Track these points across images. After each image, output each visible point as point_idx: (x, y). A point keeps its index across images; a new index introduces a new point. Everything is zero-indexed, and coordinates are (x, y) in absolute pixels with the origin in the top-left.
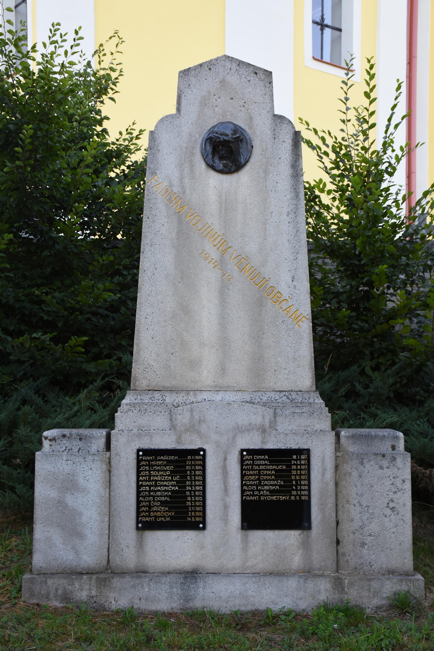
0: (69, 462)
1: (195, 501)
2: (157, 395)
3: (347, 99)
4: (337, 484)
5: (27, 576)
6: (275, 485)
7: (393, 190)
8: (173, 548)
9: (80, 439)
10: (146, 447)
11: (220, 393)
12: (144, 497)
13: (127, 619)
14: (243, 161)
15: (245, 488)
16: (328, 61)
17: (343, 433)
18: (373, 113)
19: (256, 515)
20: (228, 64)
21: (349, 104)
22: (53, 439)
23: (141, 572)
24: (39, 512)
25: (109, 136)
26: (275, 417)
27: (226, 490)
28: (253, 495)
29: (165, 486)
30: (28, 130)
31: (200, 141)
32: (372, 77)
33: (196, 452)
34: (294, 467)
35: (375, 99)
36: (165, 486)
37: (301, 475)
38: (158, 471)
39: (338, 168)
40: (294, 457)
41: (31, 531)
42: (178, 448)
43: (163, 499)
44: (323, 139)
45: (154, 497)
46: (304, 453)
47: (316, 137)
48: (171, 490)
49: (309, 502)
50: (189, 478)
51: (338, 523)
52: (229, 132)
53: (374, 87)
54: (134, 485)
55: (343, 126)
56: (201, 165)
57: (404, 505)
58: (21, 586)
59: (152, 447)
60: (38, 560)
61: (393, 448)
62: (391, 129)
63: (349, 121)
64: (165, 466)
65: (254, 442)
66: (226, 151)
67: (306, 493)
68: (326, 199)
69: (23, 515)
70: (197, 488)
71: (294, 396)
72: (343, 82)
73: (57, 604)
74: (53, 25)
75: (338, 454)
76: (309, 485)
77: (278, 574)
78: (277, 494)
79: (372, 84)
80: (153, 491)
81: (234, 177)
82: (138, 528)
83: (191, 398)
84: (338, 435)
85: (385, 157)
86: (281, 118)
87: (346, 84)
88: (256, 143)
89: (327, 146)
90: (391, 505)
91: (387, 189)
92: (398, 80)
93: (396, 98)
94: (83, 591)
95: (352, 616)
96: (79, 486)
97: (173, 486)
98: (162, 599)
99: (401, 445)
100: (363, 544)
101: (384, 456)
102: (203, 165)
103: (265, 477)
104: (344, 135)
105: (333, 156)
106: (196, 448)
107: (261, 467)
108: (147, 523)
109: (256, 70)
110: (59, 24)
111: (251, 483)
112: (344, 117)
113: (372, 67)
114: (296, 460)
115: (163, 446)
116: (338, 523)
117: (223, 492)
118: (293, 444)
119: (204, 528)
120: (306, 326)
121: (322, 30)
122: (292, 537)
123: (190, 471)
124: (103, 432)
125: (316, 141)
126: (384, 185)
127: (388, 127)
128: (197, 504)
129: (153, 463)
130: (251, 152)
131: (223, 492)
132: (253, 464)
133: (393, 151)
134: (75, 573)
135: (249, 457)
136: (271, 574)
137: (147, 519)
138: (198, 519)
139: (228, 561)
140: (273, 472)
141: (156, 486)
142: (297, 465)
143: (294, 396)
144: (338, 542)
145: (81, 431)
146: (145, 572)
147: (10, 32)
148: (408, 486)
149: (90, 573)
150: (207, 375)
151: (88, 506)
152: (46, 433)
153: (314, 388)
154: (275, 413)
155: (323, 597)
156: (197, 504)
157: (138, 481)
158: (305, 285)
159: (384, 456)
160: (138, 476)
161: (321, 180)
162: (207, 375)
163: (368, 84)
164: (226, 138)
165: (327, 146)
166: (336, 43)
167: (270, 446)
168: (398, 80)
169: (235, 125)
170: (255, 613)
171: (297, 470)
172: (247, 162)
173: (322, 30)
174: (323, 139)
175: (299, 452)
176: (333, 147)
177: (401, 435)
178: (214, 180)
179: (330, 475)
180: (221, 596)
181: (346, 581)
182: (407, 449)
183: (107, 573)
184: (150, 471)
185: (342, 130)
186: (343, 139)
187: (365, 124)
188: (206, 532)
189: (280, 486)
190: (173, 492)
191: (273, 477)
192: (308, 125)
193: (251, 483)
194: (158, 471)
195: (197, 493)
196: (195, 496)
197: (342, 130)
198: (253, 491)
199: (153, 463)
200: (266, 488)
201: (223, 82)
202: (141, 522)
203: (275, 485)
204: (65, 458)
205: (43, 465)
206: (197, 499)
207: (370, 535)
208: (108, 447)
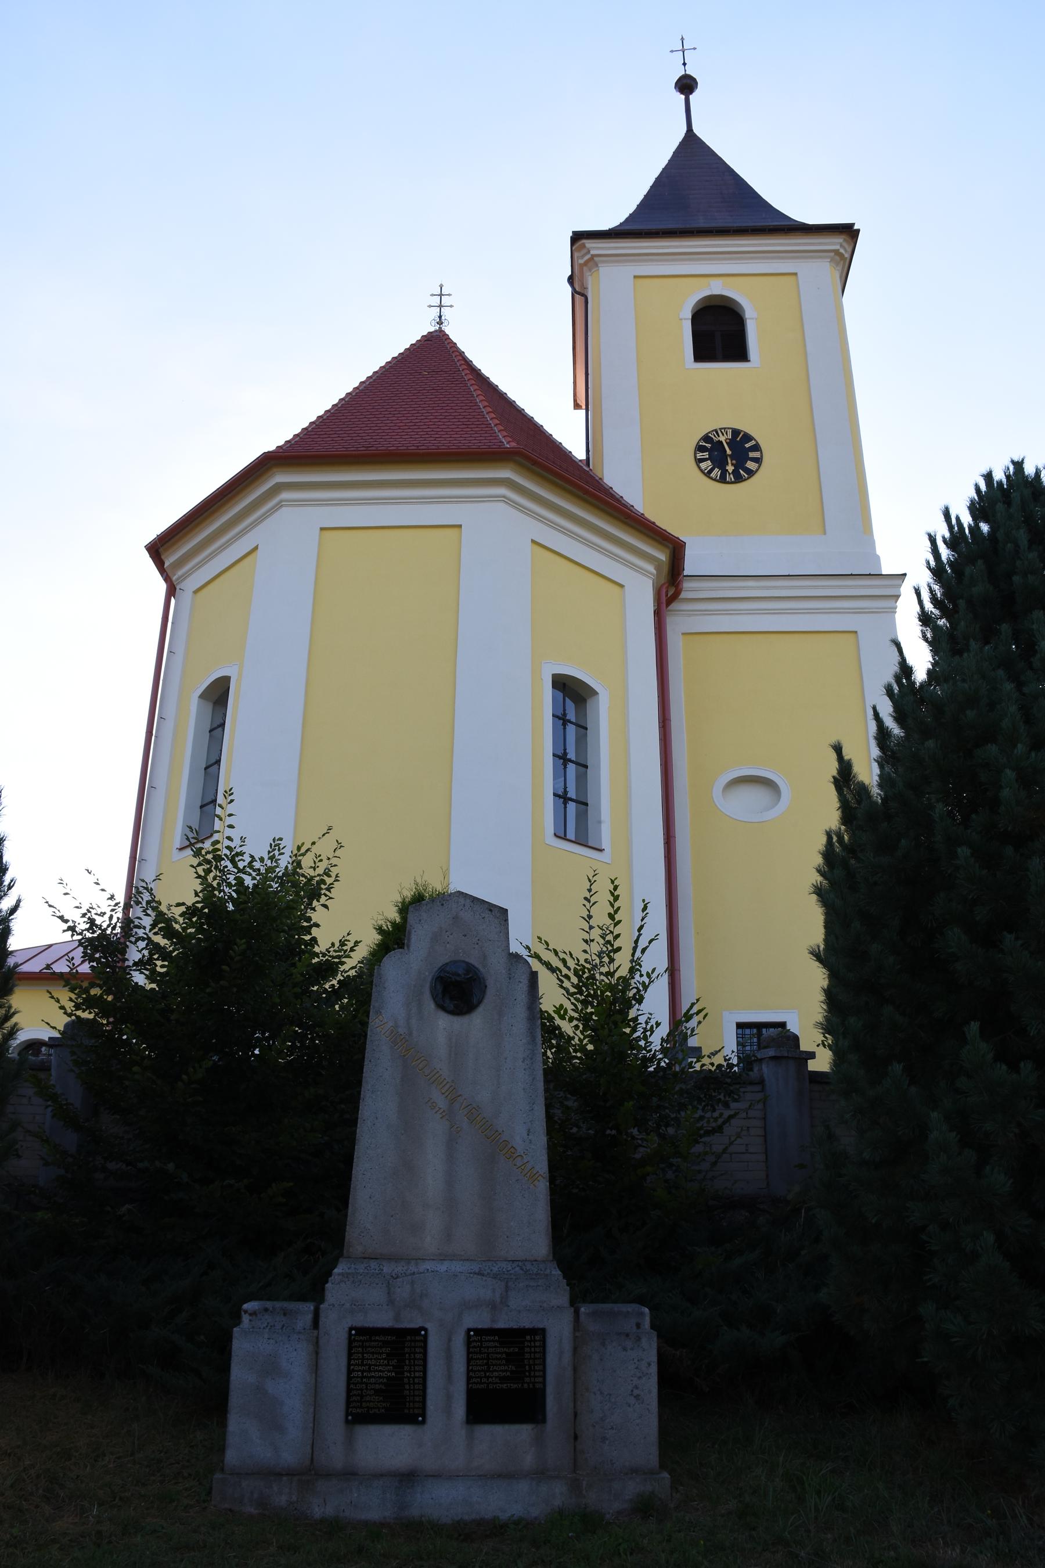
0: (272, 1341)
1: (414, 1390)
2: (373, 1264)
3: (590, 917)
4: (575, 1369)
5: (218, 1476)
6: (506, 1371)
7: (642, 1020)
8: (388, 1446)
9: (285, 1314)
10: (359, 1325)
11: (446, 1262)
12: (355, 1384)
13: (333, 1527)
14: (475, 1001)
15: (471, 1374)
16: (573, 839)
17: (582, 1309)
18: (618, 936)
20: (462, 900)
21: (592, 922)
22: (253, 1314)
23: (350, 1474)
24: (235, 1400)
26: (507, 1292)
27: (449, 1378)
28: (481, 1383)
29: (380, 1371)
30: (242, 944)
31: (429, 979)
32: (616, 898)
33: (416, 1331)
34: (527, 1350)
35: (619, 922)
36: (380, 1371)
37: (535, 1359)
38: (373, 1353)
39: (581, 993)
40: (528, 1338)
41: (223, 1423)
42: (397, 1326)
43: (377, 1387)
44: (564, 961)
45: (367, 1384)
46: (539, 1334)
47: (556, 959)
48: (386, 1378)
50: (407, 1362)
51: (576, 1415)
52: (461, 972)
53: (619, 908)
54: (344, 1370)
55: (586, 947)
56: (430, 1005)
57: (650, 1392)
58: (211, 1488)
59: (366, 1325)
60: (231, 1456)
61: (638, 1326)
62: (638, 954)
63: (593, 941)
64: (381, 1347)
65: (480, 1319)
66: (458, 990)
67: (541, 1379)
68: (567, 1027)
69: (214, 1404)
70: (417, 1374)
71: (528, 1266)
72: (586, 898)
73: (252, 1510)
74: (274, 840)
75: (577, 1334)
76: (544, 1371)
77: (507, 1475)
78: (507, 1382)
79: (616, 905)
80: (365, 1377)
82: (347, 1422)
83: (413, 1268)
84: (577, 1312)
85: (632, 981)
86: (517, 957)
87: (589, 901)
88: (490, 983)
89: (569, 969)
90: (636, 1392)
91: (635, 1019)
92: (644, 901)
93: (642, 920)
94: (282, 1496)
95: (589, 1521)
96: (280, 1376)
97: (389, 1371)
98: (373, 1506)
99: (647, 1319)
100: (604, 1439)
101: (627, 1335)
102: (433, 1006)
103: (494, 1362)
104: (588, 956)
105: (575, 980)
106: (417, 1326)
107: (491, 1350)
109: (491, 907)
110: (281, 839)
111: (479, 1368)
112: (586, 937)
113: (616, 888)
114: (530, 1341)
115: (379, 1324)
116: (576, 1415)
117: (446, 1380)
118: (526, 1322)
119: (424, 1422)
120: (542, 1187)
121: (565, 804)
122: (524, 1432)
123: (410, 1354)
124: (311, 1307)
125: (556, 963)
126: (632, 1013)
127: (635, 949)
128: (417, 1393)
129: (368, 1344)
131: (446, 1380)
132: (481, 1346)
133: (641, 976)
134: (272, 1474)
135: (477, 1338)
136: (499, 1476)
137: (359, 1410)
138: (416, 1411)
139: (450, 1462)
140: (504, 1356)
141: (369, 1371)
142: (530, 1347)
143: (528, 1266)
144: (576, 1438)
145: (286, 1304)
146: (354, 1474)
147: (228, 848)
148: (654, 1369)
149: (290, 1473)
150: (430, 1241)
151: (291, 1393)
152: (245, 1306)
153: (551, 1258)
154: (507, 1286)
155: (557, 1502)
156: (417, 1393)
157: (349, 1365)
158: (541, 1140)
159: (627, 1335)
160: (349, 1360)
161: (561, 1006)
162: (430, 1241)
163: (613, 906)
164: (458, 979)
165: (569, 969)
166: (582, 818)
167: (501, 1325)
168: (644, 901)
169: (468, 964)
170: (480, 1522)
171: (530, 1353)
172: (480, 1002)
173: (565, 804)
174: (564, 961)
176: (575, 969)
177: (646, 1310)
178: (444, 1023)
179: (567, 1358)
180: (443, 1501)
181: (584, 1483)
182: (653, 1326)
183: (310, 1473)
184: (363, 1354)
185: (585, 951)
186: (586, 960)
187: (611, 951)
188: (426, 1426)
189: (512, 1372)
190: (388, 1378)
191: (504, 1362)
192: (548, 945)
193: (479, 1368)
194: (373, 1353)
195: (416, 1380)
196: (414, 1384)
197: (585, 951)
198: (481, 1378)
199: (368, 1344)
200: (496, 1374)
201: (456, 918)
202: (351, 1414)
203: (506, 1371)
204: (266, 1336)
205: (242, 1345)
206: (416, 1387)
207: (612, 1428)
208: (316, 1323)
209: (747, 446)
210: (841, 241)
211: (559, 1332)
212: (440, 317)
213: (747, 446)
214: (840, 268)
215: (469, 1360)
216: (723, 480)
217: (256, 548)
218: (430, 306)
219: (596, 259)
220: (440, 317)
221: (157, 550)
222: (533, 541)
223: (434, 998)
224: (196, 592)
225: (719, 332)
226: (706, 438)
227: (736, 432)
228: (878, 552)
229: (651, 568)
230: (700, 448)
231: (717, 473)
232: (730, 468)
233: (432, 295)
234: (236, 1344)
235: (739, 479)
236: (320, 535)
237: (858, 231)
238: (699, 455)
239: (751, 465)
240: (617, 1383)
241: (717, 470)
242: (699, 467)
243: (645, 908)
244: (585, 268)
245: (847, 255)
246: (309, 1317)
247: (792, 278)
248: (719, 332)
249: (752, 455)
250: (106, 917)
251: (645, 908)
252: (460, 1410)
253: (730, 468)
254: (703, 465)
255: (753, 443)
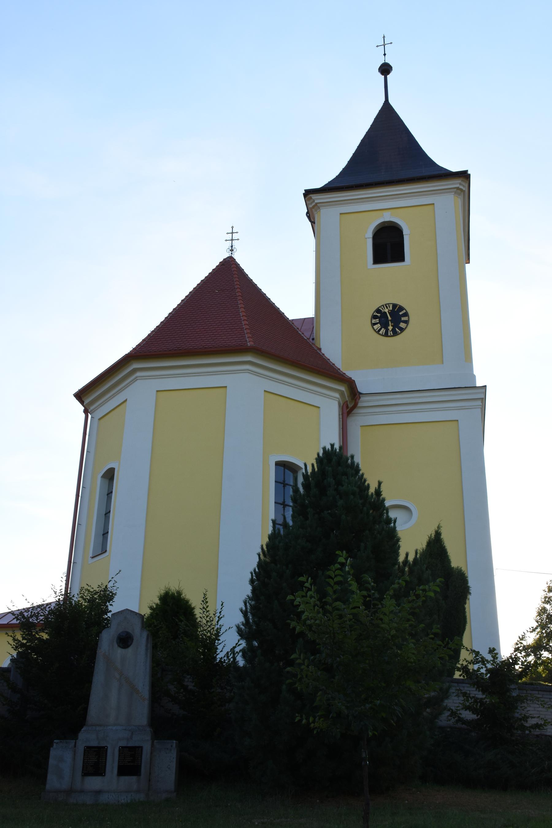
8: (94, 783)
19: (123, 771)
23: (82, 791)
25: (318, 454)
33: (104, 747)
49: (141, 766)
51: (150, 774)
60: (48, 787)
61: (172, 746)
65: (123, 744)
76: (141, 759)
81: (126, 650)
96: (63, 761)
102: (117, 646)
108: (86, 773)
115: (94, 745)
116: (150, 774)
117: (112, 762)
119: (104, 775)
122: (134, 778)
130: (132, 641)
131: (112, 762)
144: (150, 781)
167: (129, 745)
172: (131, 644)
175: (139, 747)
178: (120, 651)
205: (53, 753)
208: (75, 746)
209: (401, 313)
210: (460, 181)
211: (147, 748)
212: (232, 246)
213: (401, 313)
214: (462, 197)
215: (119, 756)
216: (386, 335)
217: (126, 400)
218: (226, 240)
219: (318, 205)
220: (232, 246)
221: (80, 396)
222: (265, 391)
223: (117, 643)
224: (100, 419)
225: (388, 244)
226: (378, 311)
227: (394, 306)
228: (475, 373)
229: (337, 395)
230: (374, 317)
231: (383, 331)
232: (390, 328)
233: (228, 233)
234: (51, 752)
235: (395, 334)
236: (156, 394)
237: (470, 175)
238: (374, 321)
239: (402, 325)
240: (165, 764)
241: (383, 329)
242: (373, 328)
243: (222, 605)
244: (313, 210)
245: (465, 189)
246: (73, 744)
247: (431, 207)
248: (388, 244)
249: (403, 319)
250: (30, 613)
251: (222, 605)
252: (116, 771)
253: (390, 328)
254: (376, 327)
255: (404, 311)
